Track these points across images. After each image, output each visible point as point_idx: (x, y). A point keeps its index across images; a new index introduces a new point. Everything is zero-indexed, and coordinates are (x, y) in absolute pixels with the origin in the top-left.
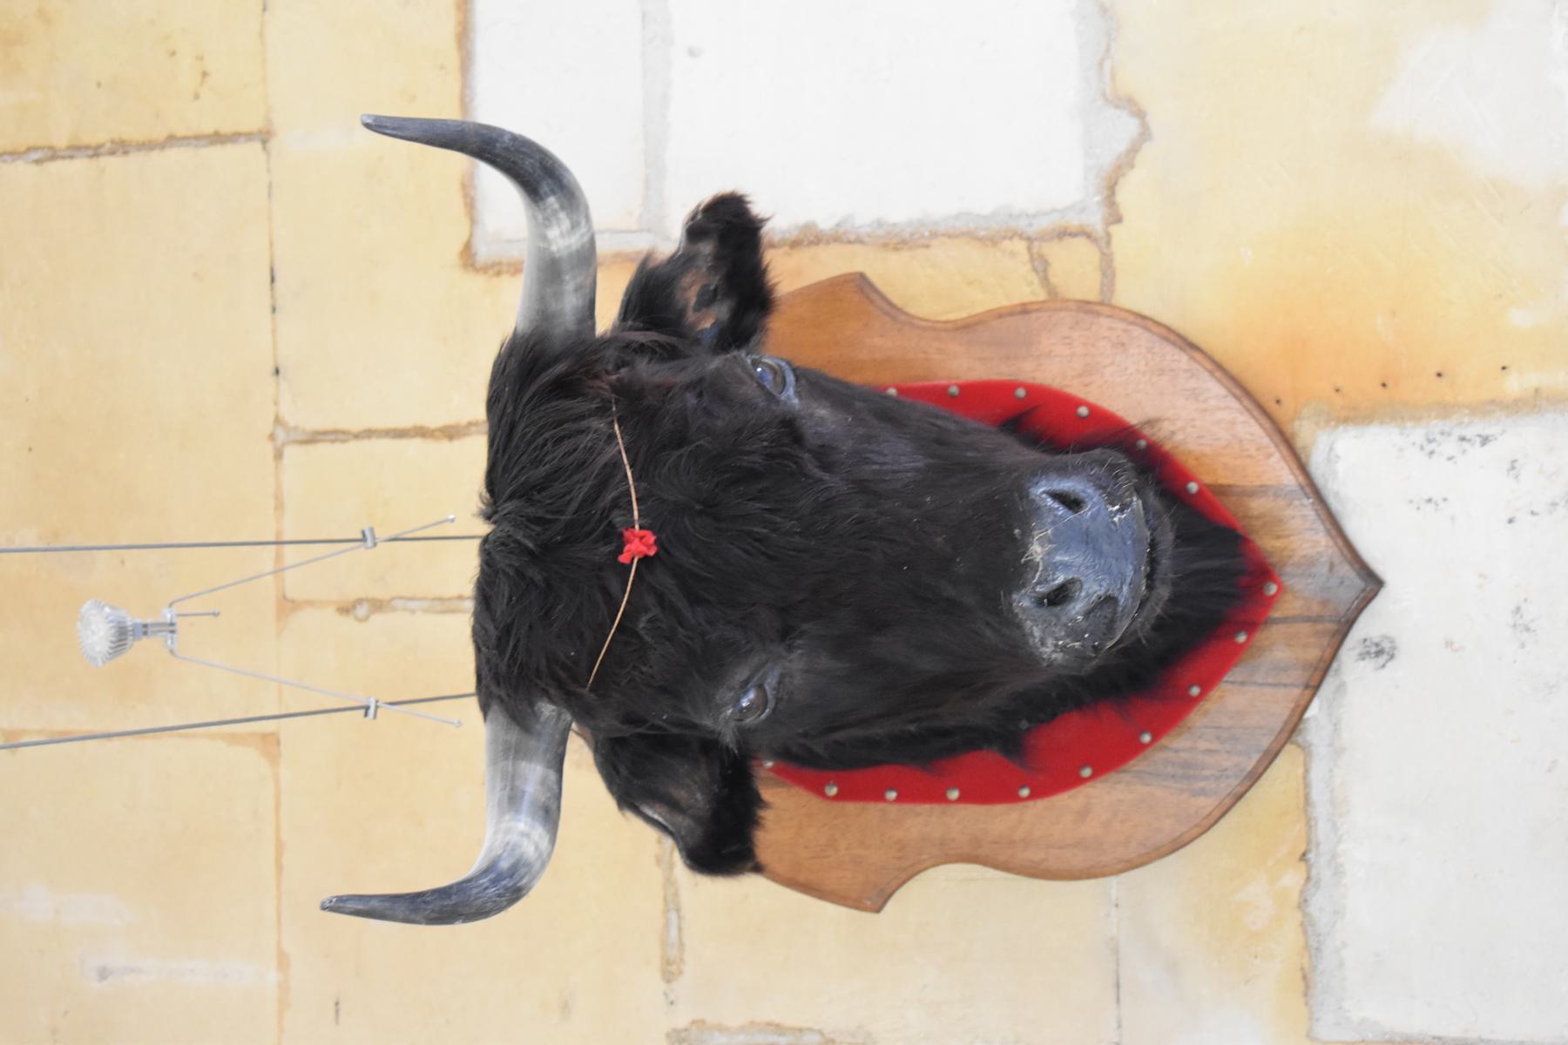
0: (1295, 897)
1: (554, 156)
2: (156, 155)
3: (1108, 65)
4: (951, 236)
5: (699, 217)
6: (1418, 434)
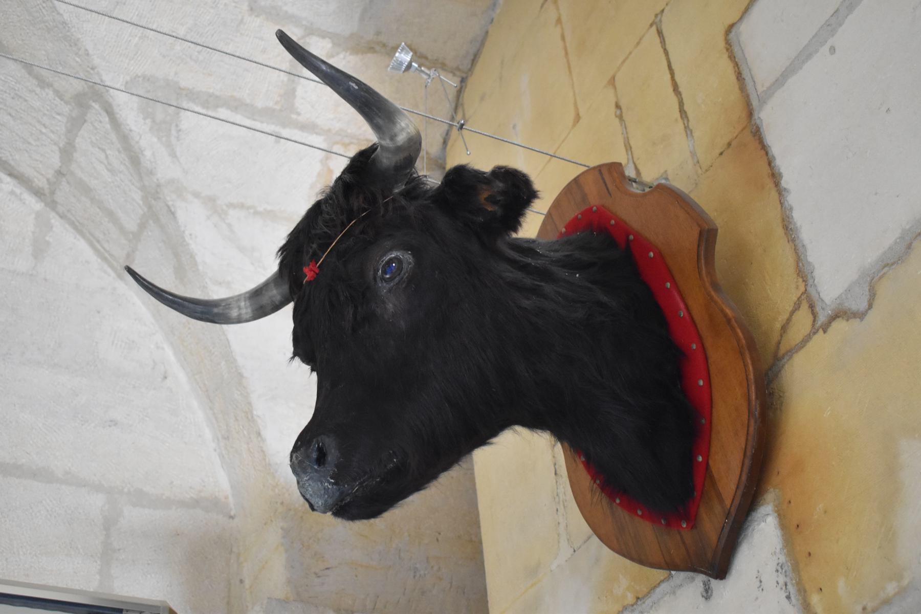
0: (626, 603)
1: (359, 112)
2: (96, 10)
3: (886, 269)
4: (796, 250)
5: (503, 170)
6: (783, 559)
